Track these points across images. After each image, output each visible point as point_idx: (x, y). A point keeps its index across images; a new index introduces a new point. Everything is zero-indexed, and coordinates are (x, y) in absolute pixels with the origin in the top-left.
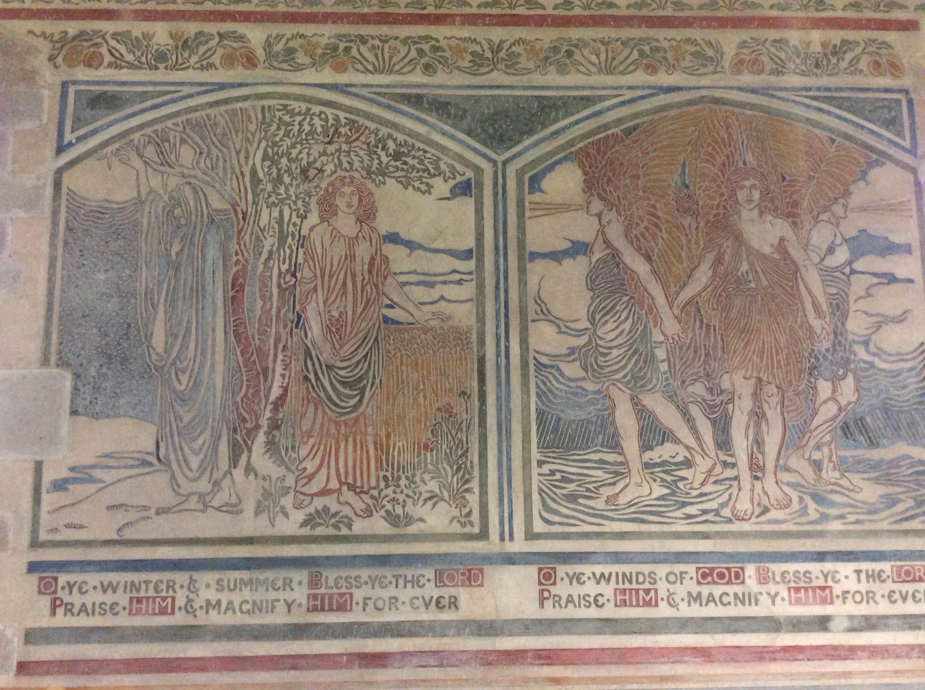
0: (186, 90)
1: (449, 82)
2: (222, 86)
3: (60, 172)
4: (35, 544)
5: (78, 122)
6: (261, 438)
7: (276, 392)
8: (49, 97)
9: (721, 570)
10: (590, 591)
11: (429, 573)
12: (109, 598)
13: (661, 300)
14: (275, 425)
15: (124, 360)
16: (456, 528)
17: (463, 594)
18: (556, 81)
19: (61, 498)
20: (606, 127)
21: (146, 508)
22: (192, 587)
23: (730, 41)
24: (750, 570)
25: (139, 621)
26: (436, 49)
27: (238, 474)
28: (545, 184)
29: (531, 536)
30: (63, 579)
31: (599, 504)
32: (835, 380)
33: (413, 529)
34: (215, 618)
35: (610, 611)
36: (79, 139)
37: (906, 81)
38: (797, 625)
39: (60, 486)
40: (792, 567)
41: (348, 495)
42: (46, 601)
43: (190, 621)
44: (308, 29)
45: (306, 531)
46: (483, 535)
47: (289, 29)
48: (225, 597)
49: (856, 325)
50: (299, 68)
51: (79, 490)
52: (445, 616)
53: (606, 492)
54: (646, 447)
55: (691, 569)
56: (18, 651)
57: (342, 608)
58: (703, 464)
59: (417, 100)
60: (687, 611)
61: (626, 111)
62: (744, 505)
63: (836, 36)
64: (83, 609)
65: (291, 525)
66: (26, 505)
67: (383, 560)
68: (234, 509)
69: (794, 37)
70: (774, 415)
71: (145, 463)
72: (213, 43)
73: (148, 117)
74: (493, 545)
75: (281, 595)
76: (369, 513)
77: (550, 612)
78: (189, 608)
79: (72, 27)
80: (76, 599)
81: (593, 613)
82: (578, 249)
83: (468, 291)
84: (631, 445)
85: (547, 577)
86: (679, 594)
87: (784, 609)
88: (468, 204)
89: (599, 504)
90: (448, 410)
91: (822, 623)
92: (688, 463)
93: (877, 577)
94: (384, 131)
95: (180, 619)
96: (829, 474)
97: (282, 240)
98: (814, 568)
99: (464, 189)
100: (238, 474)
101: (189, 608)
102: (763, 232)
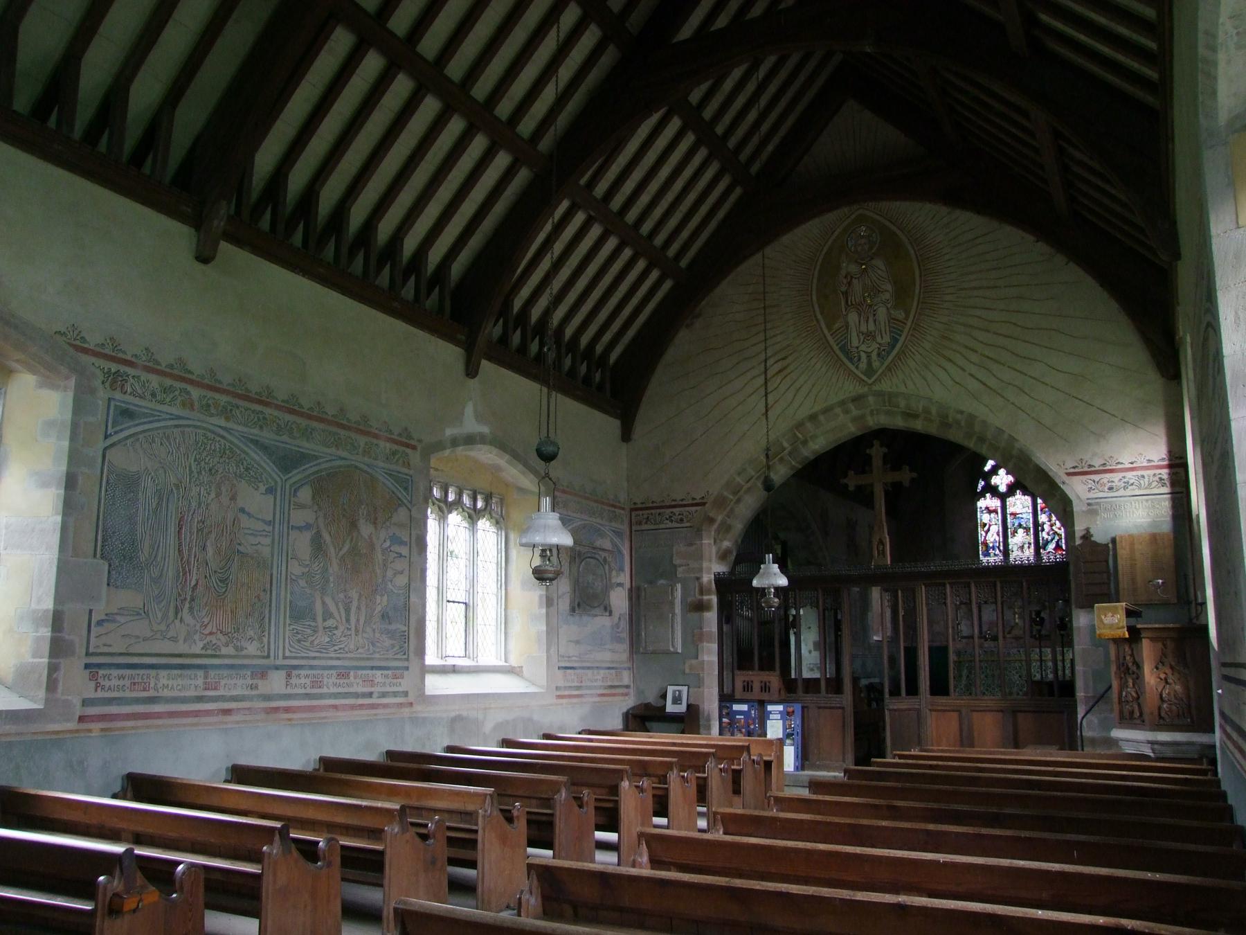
0: (164, 416)
1: (267, 436)
2: (179, 418)
3: (105, 449)
4: (87, 654)
5: (115, 423)
6: (187, 605)
7: (193, 583)
8: (101, 404)
9: (343, 675)
10: (301, 682)
11: (249, 673)
12: (121, 683)
13: (333, 554)
14: (193, 600)
15: (131, 558)
16: (259, 653)
17: (260, 682)
18: (307, 446)
19: (101, 630)
20: (321, 471)
21: (138, 637)
22: (157, 678)
23: (362, 440)
24: (352, 673)
25: (134, 695)
26: (265, 418)
27: (177, 622)
28: (299, 494)
29: (285, 658)
30: (101, 672)
31: (307, 644)
32: (382, 595)
33: (244, 652)
34: (166, 693)
35: (309, 691)
36: (116, 433)
37: (411, 472)
38: (364, 695)
39: (100, 623)
40: (364, 672)
41: (220, 636)
42: (93, 684)
43: (156, 694)
44: (217, 396)
45: (203, 652)
46: (268, 657)
47: (210, 394)
48: (170, 683)
49: (389, 573)
50: (212, 415)
51: (110, 626)
52: (254, 692)
53: (311, 639)
54: (324, 620)
55: (334, 672)
56: (78, 711)
57: (216, 689)
58: (341, 628)
59: (256, 442)
60: (335, 690)
61: (329, 465)
62: (352, 647)
63: (395, 447)
64: (110, 689)
65: (197, 649)
66: (85, 633)
67: (232, 667)
68: (174, 639)
69: (382, 444)
70: (363, 609)
71: (138, 614)
72: (177, 393)
73: (147, 427)
74: (270, 662)
75: (192, 682)
76: (227, 645)
77: (289, 691)
78: (156, 690)
79: (114, 367)
80: (107, 683)
81: (303, 691)
82: (308, 527)
83: (268, 541)
84: (320, 619)
85: (289, 676)
86: (331, 683)
87: (361, 689)
88: (271, 498)
89: (307, 644)
90: (258, 597)
91: (370, 695)
92: (336, 628)
93: (386, 676)
94: (243, 456)
95: (152, 693)
96: (377, 635)
97: (200, 504)
98: (370, 672)
99: (271, 491)
100: (177, 622)
101: (156, 690)
102: (366, 529)
